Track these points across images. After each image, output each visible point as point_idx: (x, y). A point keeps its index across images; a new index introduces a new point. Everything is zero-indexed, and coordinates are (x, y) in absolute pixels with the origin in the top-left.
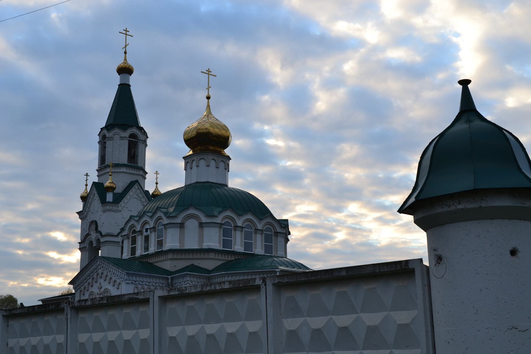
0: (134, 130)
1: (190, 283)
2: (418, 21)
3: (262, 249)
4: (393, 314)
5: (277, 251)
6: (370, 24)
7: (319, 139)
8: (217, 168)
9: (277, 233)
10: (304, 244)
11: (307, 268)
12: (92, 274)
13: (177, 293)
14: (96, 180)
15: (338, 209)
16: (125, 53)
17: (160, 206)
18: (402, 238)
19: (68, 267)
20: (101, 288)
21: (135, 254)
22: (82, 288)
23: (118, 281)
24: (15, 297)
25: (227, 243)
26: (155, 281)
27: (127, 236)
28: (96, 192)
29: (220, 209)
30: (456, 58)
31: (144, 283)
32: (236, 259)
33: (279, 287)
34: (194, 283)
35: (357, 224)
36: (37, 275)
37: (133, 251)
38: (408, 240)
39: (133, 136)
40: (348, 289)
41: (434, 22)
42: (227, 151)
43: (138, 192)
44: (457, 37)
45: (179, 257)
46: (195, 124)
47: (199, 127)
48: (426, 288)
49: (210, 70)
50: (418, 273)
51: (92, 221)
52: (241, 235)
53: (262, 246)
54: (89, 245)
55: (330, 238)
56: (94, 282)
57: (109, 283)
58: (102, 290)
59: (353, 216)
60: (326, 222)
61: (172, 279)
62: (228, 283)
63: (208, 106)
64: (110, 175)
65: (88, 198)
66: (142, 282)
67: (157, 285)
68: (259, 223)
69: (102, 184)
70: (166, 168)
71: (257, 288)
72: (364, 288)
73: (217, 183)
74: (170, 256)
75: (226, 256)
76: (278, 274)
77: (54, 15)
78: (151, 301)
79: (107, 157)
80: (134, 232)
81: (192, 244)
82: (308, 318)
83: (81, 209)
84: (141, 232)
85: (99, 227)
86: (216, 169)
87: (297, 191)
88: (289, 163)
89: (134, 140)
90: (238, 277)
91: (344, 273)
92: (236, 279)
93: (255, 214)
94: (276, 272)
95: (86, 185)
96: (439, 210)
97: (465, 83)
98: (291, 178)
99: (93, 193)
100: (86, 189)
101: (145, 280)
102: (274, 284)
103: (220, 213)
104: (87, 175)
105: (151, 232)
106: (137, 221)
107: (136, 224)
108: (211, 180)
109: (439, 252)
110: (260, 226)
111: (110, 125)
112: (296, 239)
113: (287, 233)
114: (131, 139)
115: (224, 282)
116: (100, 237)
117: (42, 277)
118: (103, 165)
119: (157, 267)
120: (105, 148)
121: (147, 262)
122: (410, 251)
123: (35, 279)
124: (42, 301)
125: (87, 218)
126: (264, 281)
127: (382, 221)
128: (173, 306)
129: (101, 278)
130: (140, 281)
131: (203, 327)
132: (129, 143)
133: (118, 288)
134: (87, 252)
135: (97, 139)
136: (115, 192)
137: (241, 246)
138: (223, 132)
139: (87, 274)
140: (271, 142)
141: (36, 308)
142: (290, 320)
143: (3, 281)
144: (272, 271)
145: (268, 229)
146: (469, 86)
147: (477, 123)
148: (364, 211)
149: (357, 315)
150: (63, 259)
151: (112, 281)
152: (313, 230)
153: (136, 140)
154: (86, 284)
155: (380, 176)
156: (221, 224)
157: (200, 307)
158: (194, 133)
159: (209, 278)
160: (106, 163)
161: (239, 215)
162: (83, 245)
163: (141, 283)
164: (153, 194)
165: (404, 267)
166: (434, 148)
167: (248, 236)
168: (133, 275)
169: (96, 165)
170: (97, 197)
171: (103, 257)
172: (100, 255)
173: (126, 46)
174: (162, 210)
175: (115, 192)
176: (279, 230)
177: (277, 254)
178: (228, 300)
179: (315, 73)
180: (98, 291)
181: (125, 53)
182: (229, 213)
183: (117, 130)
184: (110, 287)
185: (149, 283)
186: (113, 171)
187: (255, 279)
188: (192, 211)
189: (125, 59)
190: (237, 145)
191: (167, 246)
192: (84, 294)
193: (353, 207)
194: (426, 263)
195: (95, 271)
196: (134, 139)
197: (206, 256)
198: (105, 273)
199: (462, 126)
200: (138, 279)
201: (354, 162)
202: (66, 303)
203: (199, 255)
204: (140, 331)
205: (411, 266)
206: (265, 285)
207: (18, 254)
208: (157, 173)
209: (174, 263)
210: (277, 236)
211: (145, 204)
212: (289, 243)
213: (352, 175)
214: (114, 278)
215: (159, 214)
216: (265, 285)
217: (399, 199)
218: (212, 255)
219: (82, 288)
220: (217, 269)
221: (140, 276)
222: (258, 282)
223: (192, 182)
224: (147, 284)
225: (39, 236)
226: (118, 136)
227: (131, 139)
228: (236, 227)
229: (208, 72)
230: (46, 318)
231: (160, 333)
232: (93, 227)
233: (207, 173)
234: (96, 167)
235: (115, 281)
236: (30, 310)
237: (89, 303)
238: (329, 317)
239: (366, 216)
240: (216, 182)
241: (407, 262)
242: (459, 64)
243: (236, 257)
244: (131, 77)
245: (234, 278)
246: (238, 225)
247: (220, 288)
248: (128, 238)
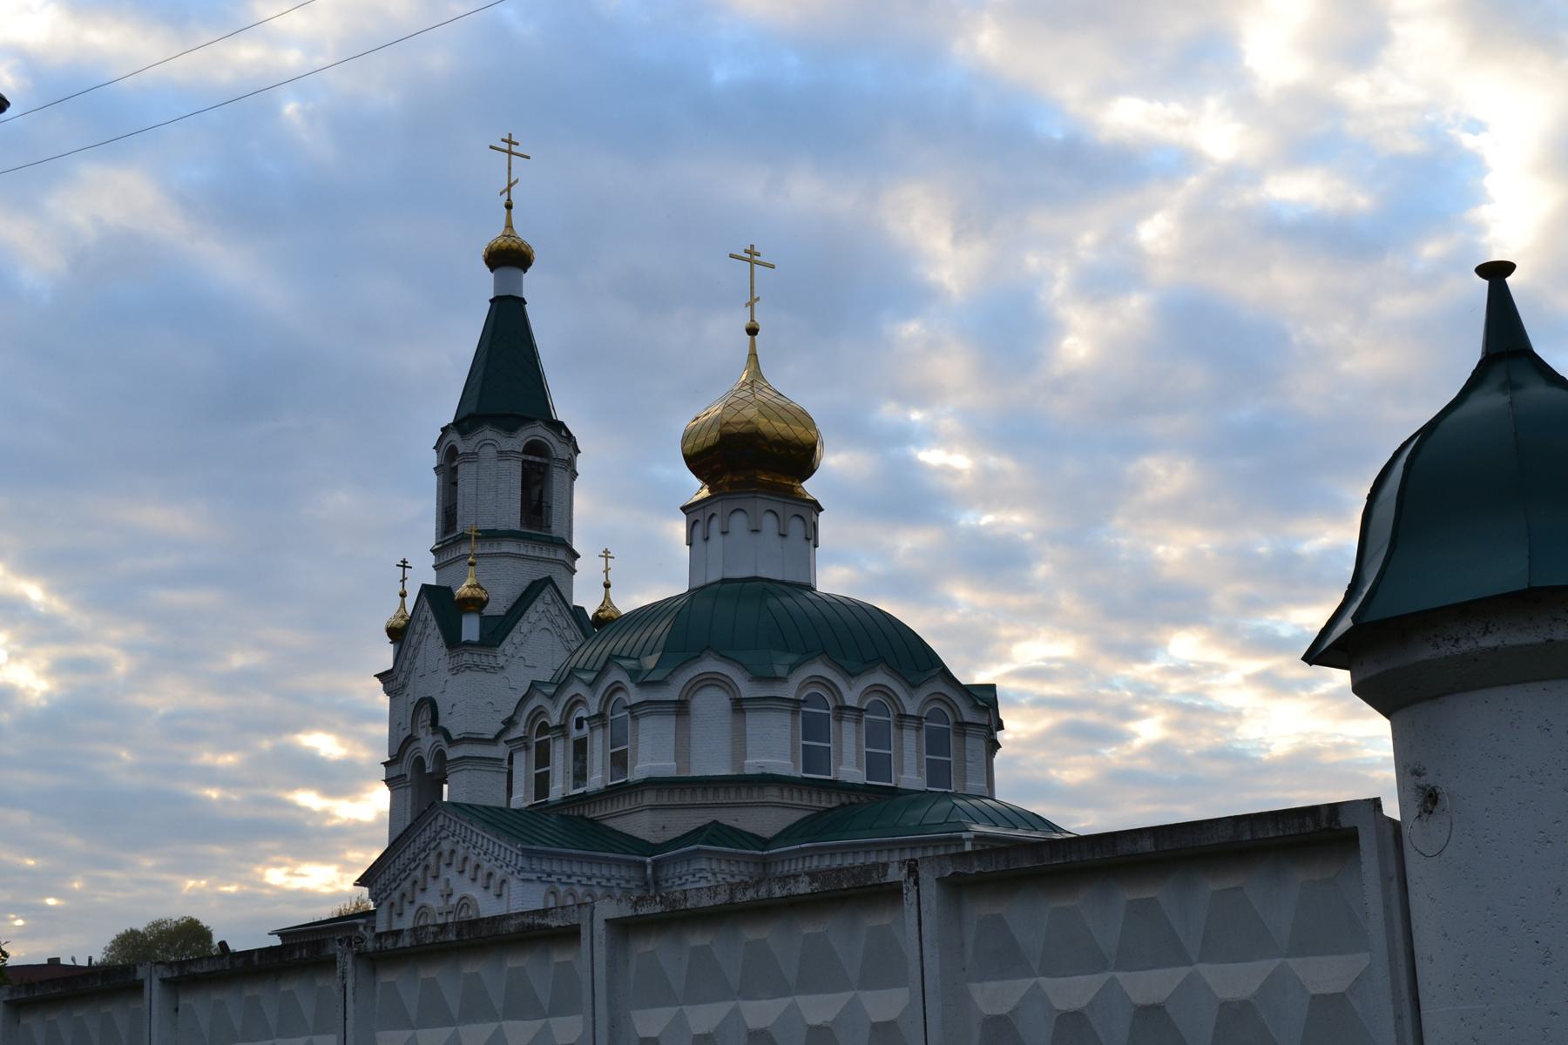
0: (539, 432)
1: (710, 876)
2: (1356, 89)
3: (919, 774)
4: (1294, 963)
6: (1212, 103)
7: (1074, 446)
8: (783, 536)
9: (962, 727)
10: (1040, 756)
11: (1054, 828)
12: (422, 856)
13: (658, 909)
15: (1139, 652)
16: (509, 206)
17: (616, 652)
18: (1335, 735)
19: (351, 833)
20: (449, 895)
22: (396, 895)
23: (499, 874)
24: (204, 923)
25: (814, 758)
26: (605, 872)
27: (523, 742)
28: (430, 615)
29: (792, 658)
30: (1476, 197)
31: (574, 880)
32: (843, 805)
33: (958, 887)
34: (720, 877)
35: (1198, 693)
36: (263, 859)
37: (542, 784)
38: (1352, 741)
39: (534, 448)
40: (1160, 893)
41: (1402, 91)
42: (810, 487)
43: (554, 610)
44: (1476, 134)
46: (716, 410)
47: (727, 418)
48: (1395, 887)
50: (1367, 842)
51: (421, 700)
52: (858, 732)
53: (919, 766)
54: (414, 770)
55: (1119, 738)
56: (429, 879)
57: (474, 880)
58: (454, 901)
59: (1183, 671)
60: (1104, 691)
61: (657, 865)
62: (807, 879)
63: (753, 355)
64: (471, 564)
66: (569, 877)
67: (613, 883)
68: (911, 696)
69: (448, 591)
70: (633, 540)
71: (892, 894)
72: (1210, 888)
73: (782, 582)
74: (649, 798)
75: (815, 797)
76: (968, 847)
77: (290, 108)
78: (585, 933)
79: (460, 513)
80: (544, 728)
81: (712, 761)
82: (1044, 981)
83: (387, 663)
84: (562, 729)
85: (442, 714)
86: (779, 539)
87: (1013, 601)
88: (987, 519)
89: (537, 459)
90: (840, 859)
91: (1147, 845)
92: (846, 864)
93: (896, 671)
94: (961, 841)
95: (403, 595)
96: (1425, 653)
97: (1496, 272)
98: (996, 562)
100: (403, 605)
101: (576, 869)
102: (940, 880)
103: (793, 668)
104: (404, 565)
106: (551, 697)
107: (547, 705)
108: (763, 573)
109: (1429, 779)
110: (911, 707)
111: (470, 417)
112: (1016, 743)
113: (994, 725)
114: (530, 458)
115: (796, 877)
117: (279, 865)
118: (451, 535)
120: (455, 484)
121: (582, 816)
122: (1362, 772)
123: (259, 869)
124: (282, 934)
125: (408, 691)
126: (913, 870)
127: (1271, 683)
128: (650, 948)
129: (449, 865)
130: (563, 873)
131: (736, 1010)
133: (499, 896)
135: (433, 459)
136: (487, 611)
137: (858, 766)
138: (798, 432)
139: (409, 854)
140: (931, 457)
141: (256, 958)
142: (992, 985)
143: (165, 877)
144: (950, 839)
145: (935, 715)
146: (1508, 280)
147: (1538, 391)
148: (1217, 655)
149: (1190, 969)
150: (337, 813)
151: (481, 875)
152: (1067, 716)
154: (407, 885)
155: (1262, 550)
156: (797, 702)
157: (726, 949)
158: (714, 435)
159: (765, 862)
160: (459, 530)
161: (850, 674)
162: (396, 771)
163: (564, 879)
164: (596, 616)
165: (1324, 825)
166: (1407, 467)
167: (877, 736)
168: (541, 855)
169: (429, 533)
171: (455, 804)
172: (445, 799)
173: (510, 185)
174: (623, 663)
175: (487, 611)
176: (968, 716)
178: (810, 928)
179: (1058, 253)
180: (441, 903)
181: (509, 206)
182: (819, 669)
183: (488, 433)
184: (475, 892)
185: (589, 878)
186: (479, 551)
187: (885, 866)
188: (710, 665)
189: (509, 226)
190: (836, 469)
191: (640, 770)
192: (400, 915)
193: (1185, 645)
194: (1392, 809)
195: (433, 845)
197: (756, 796)
198: (461, 852)
199: (1491, 400)
200: (556, 867)
201: (1180, 510)
202: (340, 941)
203: (744, 795)
204: (551, 1020)
205: (1346, 822)
206: (916, 883)
207: (208, 800)
208: (606, 555)
209: (662, 818)
211: (574, 646)
213: (1176, 549)
214: (486, 867)
215: (615, 675)
216: (916, 883)
217: (1312, 618)
218: (772, 794)
219: (396, 895)
220: (787, 835)
221: (560, 857)
222: (895, 874)
223: (710, 580)
224: (584, 881)
225: (266, 744)
226: (490, 452)
227: (530, 458)
228: (842, 709)
230: (284, 987)
231: (613, 1026)
232: (425, 716)
233: (753, 553)
234: (431, 539)
235: (490, 875)
236: (239, 962)
237: (406, 941)
238: (1106, 976)
239: (1223, 669)
240: (779, 578)
241: (1334, 809)
242: (1484, 212)
243: (844, 799)
245: (826, 862)
246: (848, 703)
247: (785, 892)
248: (527, 748)
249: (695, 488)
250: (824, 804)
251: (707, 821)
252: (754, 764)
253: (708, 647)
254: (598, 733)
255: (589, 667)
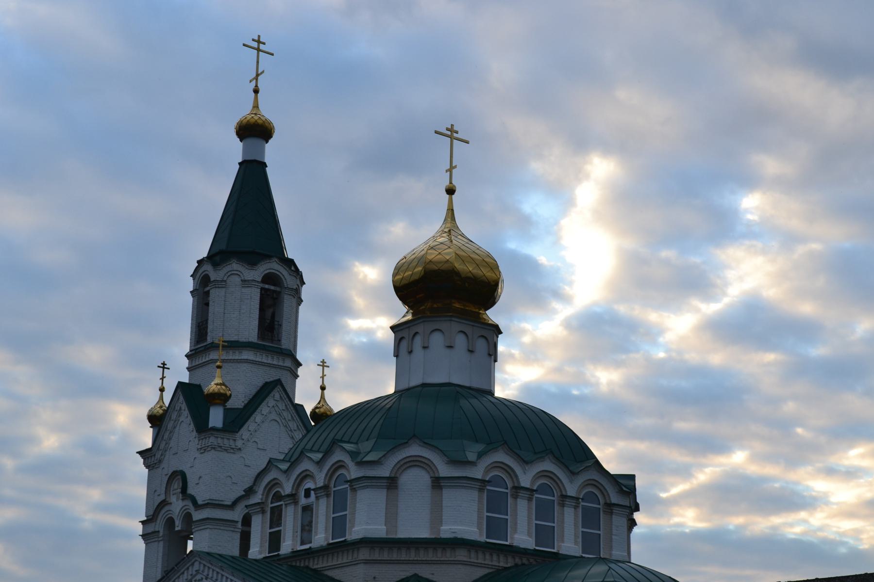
0: (273, 266)
3: (576, 543)
5: (611, 548)
8: (471, 351)
9: (610, 507)
14: (186, 379)
16: (256, 91)
17: (339, 437)
21: (278, 549)
25: (495, 527)
27: (260, 507)
28: (184, 406)
29: (480, 447)
32: (523, 564)
37: (275, 540)
39: (269, 278)
42: (493, 315)
43: (282, 406)
45: (385, 556)
49: (455, 128)
53: (576, 536)
63: (451, 211)
64: (219, 367)
65: (167, 419)
68: (571, 481)
69: (199, 387)
70: (350, 347)
73: (470, 388)
74: (364, 554)
79: (210, 327)
80: (278, 497)
83: (149, 444)
89: (272, 288)
93: (560, 460)
95: (162, 390)
99: (177, 408)
100: (161, 398)
103: (480, 455)
105: (317, 498)
107: (282, 478)
108: (455, 380)
111: (221, 253)
114: (267, 286)
116: (192, 509)
118: (202, 345)
119: (332, 579)
120: (207, 304)
121: (307, 567)
132: (261, 294)
134: (161, 544)
136: (229, 405)
138: (489, 274)
153: (278, 289)
156: (483, 481)
160: (209, 340)
161: (525, 462)
162: (151, 528)
164: (313, 413)
167: (544, 511)
170: (186, 418)
173: (258, 75)
174: (344, 445)
175: (230, 404)
176: (615, 498)
177: (611, 555)
181: (256, 91)
182: (501, 456)
183: (235, 265)
186: (224, 357)
188: (415, 450)
189: (256, 106)
191: (358, 530)
196: (274, 285)
197: (449, 555)
203: (439, 554)
210: (612, 513)
212: (636, 530)
215: (338, 456)
218: (461, 554)
223: (413, 383)
226: (236, 280)
227: (267, 286)
228: (517, 489)
229: (451, 133)
232: (177, 485)
233: (444, 364)
234: (187, 349)
240: (467, 384)
243: (518, 561)
244: (267, 145)
246: (523, 485)
248: (263, 512)
249: (400, 312)
250: (502, 564)
251: (408, 574)
252: (447, 530)
253: (414, 436)
254: (323, 502)
255: (316, 448)
